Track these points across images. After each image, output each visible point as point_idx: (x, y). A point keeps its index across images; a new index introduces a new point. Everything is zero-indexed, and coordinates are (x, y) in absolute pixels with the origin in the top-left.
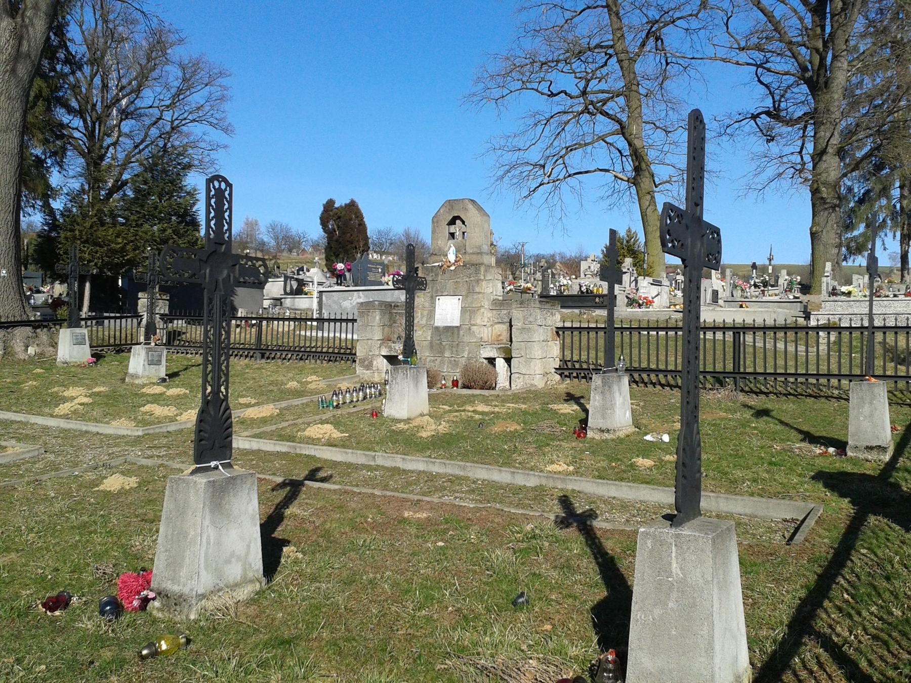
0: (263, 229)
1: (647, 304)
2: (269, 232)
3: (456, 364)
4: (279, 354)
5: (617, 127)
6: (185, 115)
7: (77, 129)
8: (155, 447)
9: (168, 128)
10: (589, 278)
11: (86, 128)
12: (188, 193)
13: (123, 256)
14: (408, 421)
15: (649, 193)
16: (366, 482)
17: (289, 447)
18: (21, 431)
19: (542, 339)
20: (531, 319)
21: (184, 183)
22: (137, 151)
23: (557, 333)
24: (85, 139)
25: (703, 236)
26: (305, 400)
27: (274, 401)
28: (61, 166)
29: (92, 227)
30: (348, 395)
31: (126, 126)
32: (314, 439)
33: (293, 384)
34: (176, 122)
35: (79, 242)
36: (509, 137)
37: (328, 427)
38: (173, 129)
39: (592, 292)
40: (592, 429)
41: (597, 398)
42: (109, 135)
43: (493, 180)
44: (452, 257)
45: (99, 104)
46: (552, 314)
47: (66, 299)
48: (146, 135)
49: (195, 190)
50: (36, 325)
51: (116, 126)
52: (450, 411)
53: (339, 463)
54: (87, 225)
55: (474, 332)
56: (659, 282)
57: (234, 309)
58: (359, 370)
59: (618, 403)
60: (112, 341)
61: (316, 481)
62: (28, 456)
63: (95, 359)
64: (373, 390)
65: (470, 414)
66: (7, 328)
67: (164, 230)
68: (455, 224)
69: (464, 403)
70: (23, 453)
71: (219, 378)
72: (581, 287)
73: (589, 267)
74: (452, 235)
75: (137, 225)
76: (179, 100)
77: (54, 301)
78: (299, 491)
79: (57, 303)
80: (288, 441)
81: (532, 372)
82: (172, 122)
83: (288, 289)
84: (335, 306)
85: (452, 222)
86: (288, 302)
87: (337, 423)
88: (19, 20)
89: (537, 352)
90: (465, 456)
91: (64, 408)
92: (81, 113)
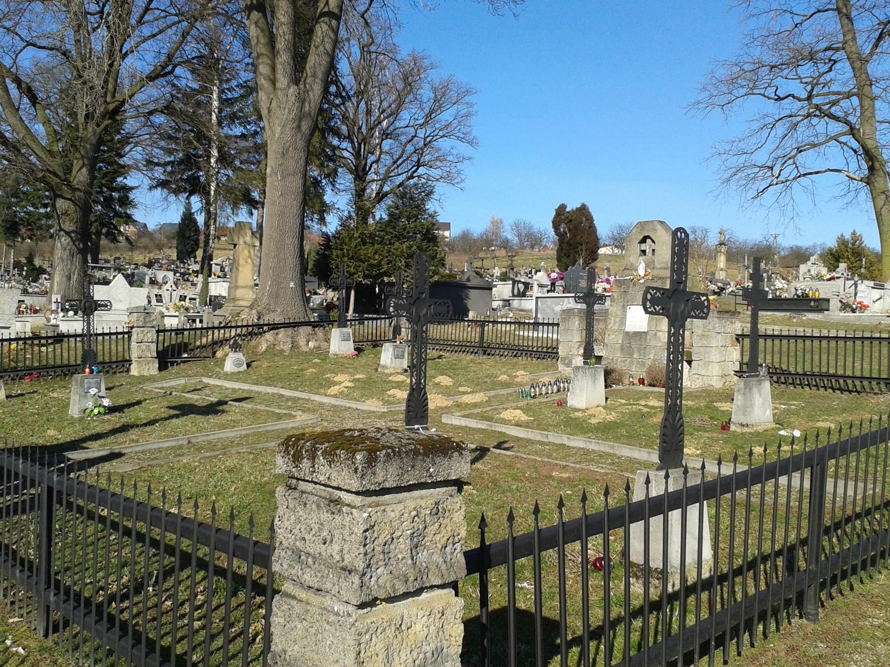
0: (507, 227)
1: (861, 308)
2: (512, 229)
3: (643, 364)
4: (498, 351)
5: (847, 128)
6: (436, 133)
7: (346, 149)
8: (395, 420)
9: (421, 144)
10: (808, 281)
11: (354, 148)
12: (430, 215)
13: (379, 270)
14: (583, 411)
15: (883, 193)
16: (536, 453)
17: (487, 425)
18: (305, 405)
19: (720, 344)
20: (710, 327)
21: (427, 207)
22: (395, 166)
23: (737, 340)
24: (352, 158)
25: (688, 300)
26: (510, 390)
27: (485, 390)
28: (333, 185)
29: (356, 247)
30: (550, 387)
31: (387, 144)
32: (506, 420)
33: (503, 378)
34: (428, 139)
35: (346, 258)
36: (734, 141)
37: (518, 412)
38: (425, 145)
39: (807, 295)
40: (735, 424)
41: (740, 398)
42: (372, 153)
43: (718, 183)
44: (641, 272)
45: (364, 127)
46: (731, 322)
47: (337, 303)
48: (403, 151)
49: (435, 213)
50: (314, 325)
51: (377, 144)
52: (626, 404)
53: (522, 439)
54: (353, 245)
55: (659, 337)
56: (881, 285)
57: (466, 312)
58: (561, 367)
59: (757, 403)
60: (370, 337)
61: (501, 449)
62: (310, 422)
63: (357, 352)
64: (566, 384)
65: (640, 407)
66: (294, 327)
67: (411, 247)
68: (645, 242)
69: (640, 398)
70: (307, 420)
71: (420, 375)
72: (797, 290)
73: (809, 271)
74: (644, 252)
75: (390, 244)
76: (431, 119)
77: (327, 304)
78: (485, 455)
79: (330, 306)
80: (487, 421)
81: (710, 374)
82: (425, 139)
83: (516, 292)
84: (548, 310)
85: (644, 240)
86: (515, 303)
87: (526, 410)
88: (302, 86)
89: (715, 356)
90: (618, 439)
91: (334, 390)
92: (349, 138)
